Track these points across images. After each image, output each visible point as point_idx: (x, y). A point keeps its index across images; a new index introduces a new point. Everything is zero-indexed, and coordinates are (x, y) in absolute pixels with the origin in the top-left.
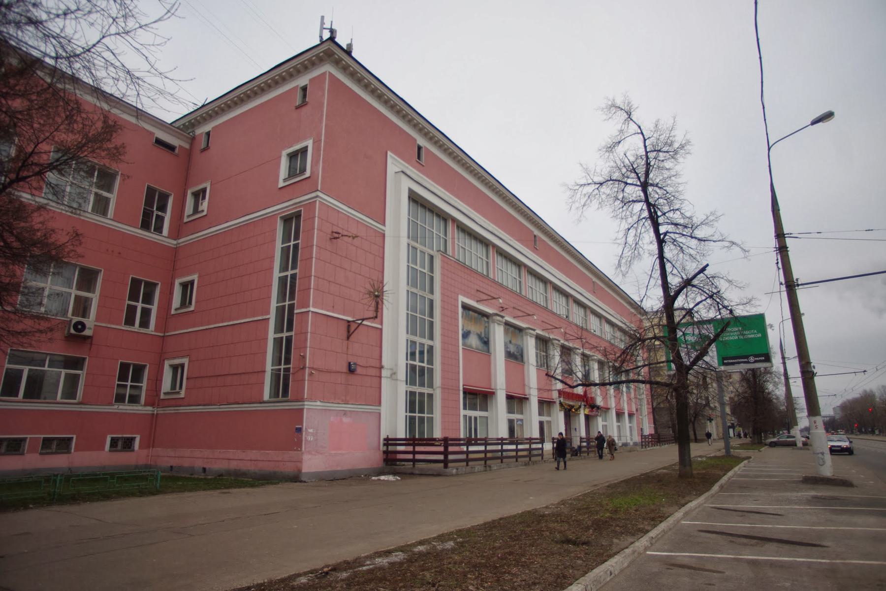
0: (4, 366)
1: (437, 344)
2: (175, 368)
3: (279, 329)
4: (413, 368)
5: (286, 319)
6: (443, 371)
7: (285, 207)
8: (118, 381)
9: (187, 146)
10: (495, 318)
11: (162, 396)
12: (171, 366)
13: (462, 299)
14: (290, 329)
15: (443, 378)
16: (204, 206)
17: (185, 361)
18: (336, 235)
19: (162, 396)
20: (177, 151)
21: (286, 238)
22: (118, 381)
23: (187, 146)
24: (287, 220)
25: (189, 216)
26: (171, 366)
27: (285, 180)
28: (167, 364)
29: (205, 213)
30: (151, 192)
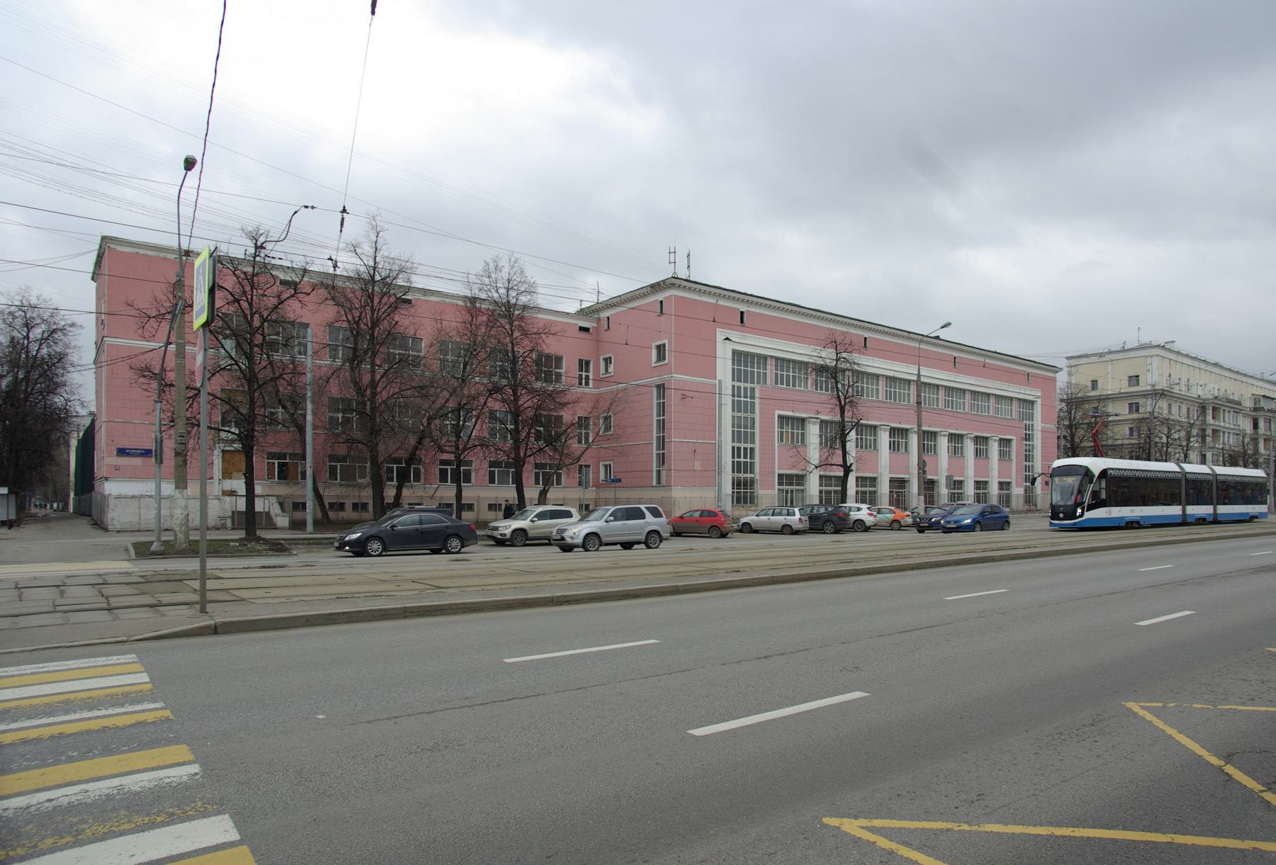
0: (774, 473)
1: (757, 446)
2: (606, 466)
3: (658, 449)
4: (739, 463)
5: (662, 443)
6: (761, 463)
7: (655, 380)
8: (447, 482)
9: (596, 325)
10: (810, 420)
11: (601, 482)
12: (603, 465)
13: (778, 412)
14: (663, 415)
15: (760, 467)
16: (611, 369)
17: (611, 463)
18: (684, 396)
19: (601, 482)
20: (591, 331)
21: (659, 397)
22: (447, 482)
23: (596, 325)
24: (658, 387)
25: (603, 374)
26: (603, 465)
27: (655, 363)
28: (601, 464)
29: (612, 374)
30: (581, 361)
